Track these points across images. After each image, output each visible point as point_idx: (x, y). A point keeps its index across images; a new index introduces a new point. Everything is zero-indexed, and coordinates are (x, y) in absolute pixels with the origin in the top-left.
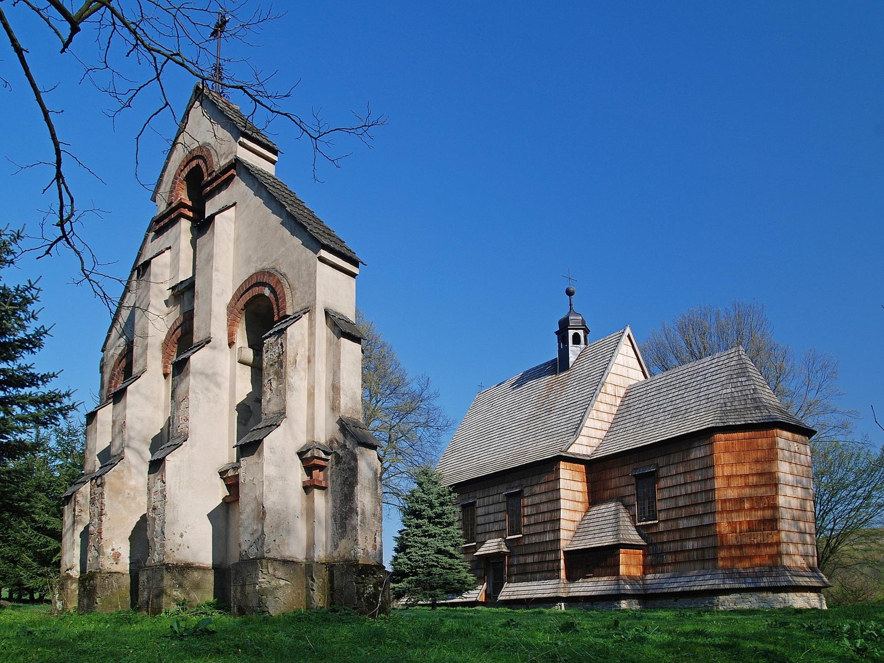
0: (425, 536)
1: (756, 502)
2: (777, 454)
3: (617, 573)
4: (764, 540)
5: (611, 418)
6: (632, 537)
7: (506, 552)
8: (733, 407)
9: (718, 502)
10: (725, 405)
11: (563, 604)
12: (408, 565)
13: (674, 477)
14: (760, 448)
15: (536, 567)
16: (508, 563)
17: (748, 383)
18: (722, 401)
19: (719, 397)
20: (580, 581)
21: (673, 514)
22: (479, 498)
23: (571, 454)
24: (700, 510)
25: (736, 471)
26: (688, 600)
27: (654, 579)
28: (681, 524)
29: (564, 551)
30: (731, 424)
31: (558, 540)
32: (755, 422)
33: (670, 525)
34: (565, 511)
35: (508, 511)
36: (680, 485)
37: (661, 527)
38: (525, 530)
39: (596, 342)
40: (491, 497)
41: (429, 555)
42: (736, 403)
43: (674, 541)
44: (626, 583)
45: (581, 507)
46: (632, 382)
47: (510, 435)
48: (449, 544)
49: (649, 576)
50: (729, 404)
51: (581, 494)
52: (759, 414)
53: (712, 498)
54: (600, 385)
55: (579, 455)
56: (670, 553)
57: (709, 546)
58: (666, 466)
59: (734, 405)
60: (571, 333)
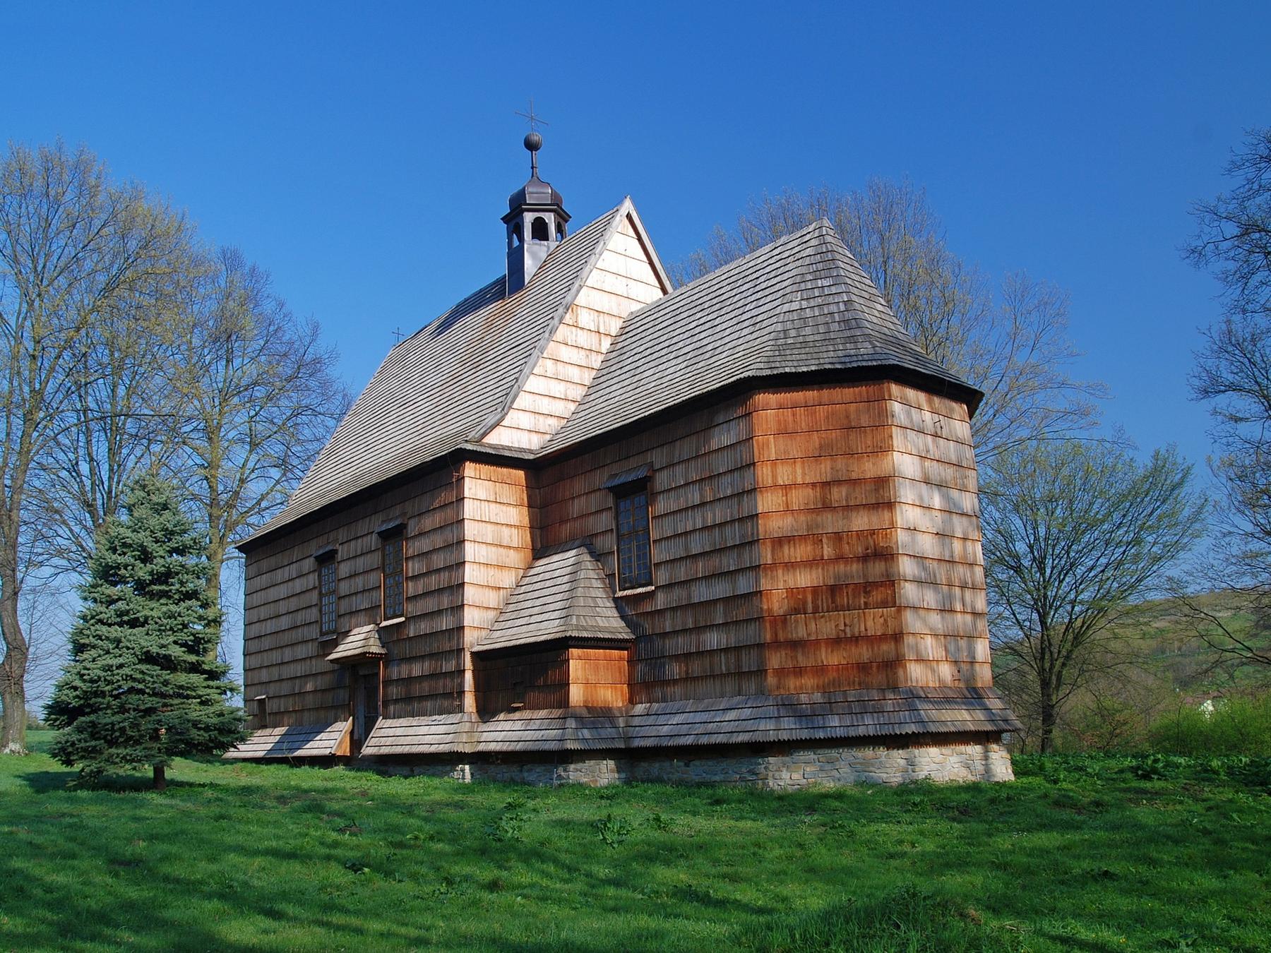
0: (121, 624)
1: (848, 543)
2: (891, 437)
3: (564, 702)
4: (866, 630)
5: (588, 378)
6: (601, 623)
7: (379, 654)
8: (801, 339)
9: (764, 543)
10: (785, 334)
11: (467, 767)
12: (76, 688)
13: (682, 491)
14: (853, 424)
15: (426, 687)
16: (384, 677)
17: (836, 289)
18: (779, 327)
19: (774, 320)
20: (502, 716)
21: (682, 573)
22: (342, 544)
23: (491, 446)
24: (730, 562)
25: (804, 474)
26: (710, 763)
27: (647, 715)
28: (696, 593)
29: (472, 653)
30: (787, 370)
31: (461, 629)
32: (839, 366)
33: (678, 596)
34: (475, 566)
35: (384, 568)
36: (693, 507)
37: (661, 601)
38: (411, 609)
39: (574, 234)
40: (360, 540)
41: (121, 666)
42: (808, 331)
43: (685, 631)
44: (583, 723)
45: (516, 559)
46: (635, 307)
47: (412, 417)
48: (171, 639)
49: (640, 708)
50: (793, 333)
51: (515, 531)
52: (852, 352)
53: (753, 534)
54: (561, 310)
55: (509, 449)
56: (676, 657)
57: (749, 643)
58: (666, 467)
59: (804, 333)
60: (529, 218)
